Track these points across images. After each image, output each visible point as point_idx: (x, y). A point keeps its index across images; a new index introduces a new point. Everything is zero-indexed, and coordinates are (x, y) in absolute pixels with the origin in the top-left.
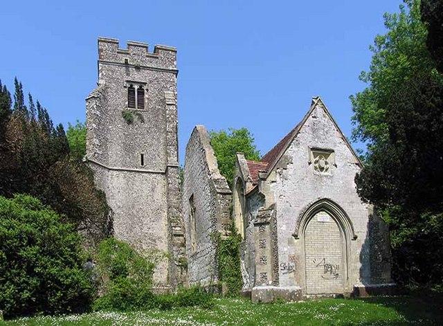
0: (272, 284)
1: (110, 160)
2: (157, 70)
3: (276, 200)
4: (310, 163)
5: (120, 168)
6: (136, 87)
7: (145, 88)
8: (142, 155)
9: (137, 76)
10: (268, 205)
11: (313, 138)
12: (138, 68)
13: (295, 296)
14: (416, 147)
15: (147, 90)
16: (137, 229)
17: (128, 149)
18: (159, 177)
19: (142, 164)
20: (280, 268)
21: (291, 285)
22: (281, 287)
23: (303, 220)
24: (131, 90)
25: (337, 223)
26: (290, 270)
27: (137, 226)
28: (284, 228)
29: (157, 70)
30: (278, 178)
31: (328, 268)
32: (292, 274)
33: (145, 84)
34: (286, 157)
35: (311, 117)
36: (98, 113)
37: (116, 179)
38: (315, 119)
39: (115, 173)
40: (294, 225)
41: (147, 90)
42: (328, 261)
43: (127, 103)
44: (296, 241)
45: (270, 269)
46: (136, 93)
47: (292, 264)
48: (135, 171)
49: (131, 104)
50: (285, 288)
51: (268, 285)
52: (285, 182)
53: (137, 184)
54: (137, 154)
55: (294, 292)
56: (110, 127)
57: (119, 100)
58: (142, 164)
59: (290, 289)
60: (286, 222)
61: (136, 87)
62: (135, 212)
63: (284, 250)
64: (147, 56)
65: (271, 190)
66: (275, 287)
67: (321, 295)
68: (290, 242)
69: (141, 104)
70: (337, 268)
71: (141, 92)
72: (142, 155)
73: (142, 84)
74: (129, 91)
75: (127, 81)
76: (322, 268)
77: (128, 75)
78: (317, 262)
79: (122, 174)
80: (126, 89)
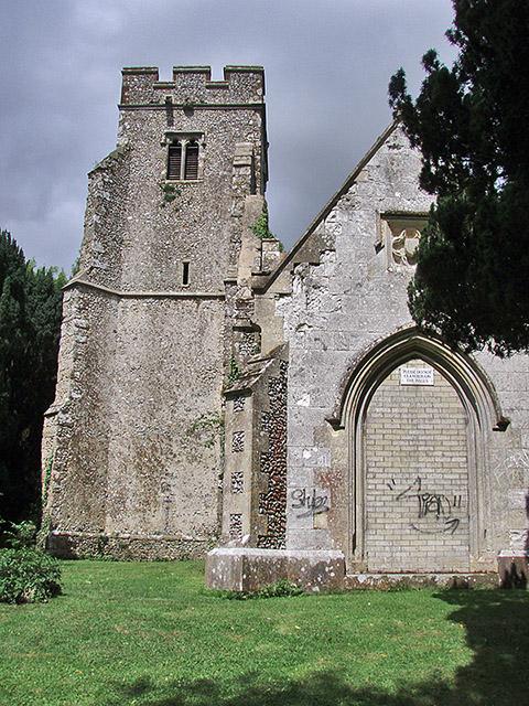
0: (249, 543)
1: (124, 278)
2: (225, 108)
3: (288, 336)
4: (379, 248)
5: (141, 293)
6: (183, 143)
7: (200, 142)
8: (186, 265)
9: (185, 124)
10: (266, 350)
11: (390, 191)
12: (189, 110)
13: (326, 575)
14: (493, 191)
15: (204, 145)
16: (165, 413)
17: (160, 255)
18: (216, 305)
19: (185, 282)
20: (290, 502)
21: (319, 548)
22: (289, 552)
23: (356, 384)
24: (174, 151)
25: (458, 391)
26: (316, 506)
27: (164, 407)
28: (305, 401)
29: (225, 108)
30: (297, 288)
31: (429, 504)
32: (322, 519)
33: (200, 134)
34: (319, 239)
35: (385, 146)
36: (106, 195)
37: (131, 314)
38: (395, 151)
39: (131, 302)
40: (333, 396)
41: (204, 145)
42: (429, 487)
43: (164, 172)
44: (335, 434)
45: (248, 504)
46: (183, 153)
47: (322, 493)
48: (168, 297)
49: (172, 170)
50: (300, 555)
51: (238, 545)
52: (315, 294)
53: (173, 321)
54: (177, 264)
55: (323, 564)
56: (130, 218)
57: (150, 165)
58: (185, 282)
59: (313, 556)
60: (312, 387)
61: (183, 143)
62: (163, 377)
63: (305, 460)
64: (207, 87)
65: (278, 313)
66: (270, 552)
67: (398, 577)
68: (319, 438)
69: (191, 169)
70: (456, 503)
71: (192, 151)
72: (186, 265)
73: (193, 138)
74: (171, 152)
75: (167, 134)
76: (414, 504)
77: (170, 123)
78: (398, 488)
79: (144, 304)
80: (166, 148)
